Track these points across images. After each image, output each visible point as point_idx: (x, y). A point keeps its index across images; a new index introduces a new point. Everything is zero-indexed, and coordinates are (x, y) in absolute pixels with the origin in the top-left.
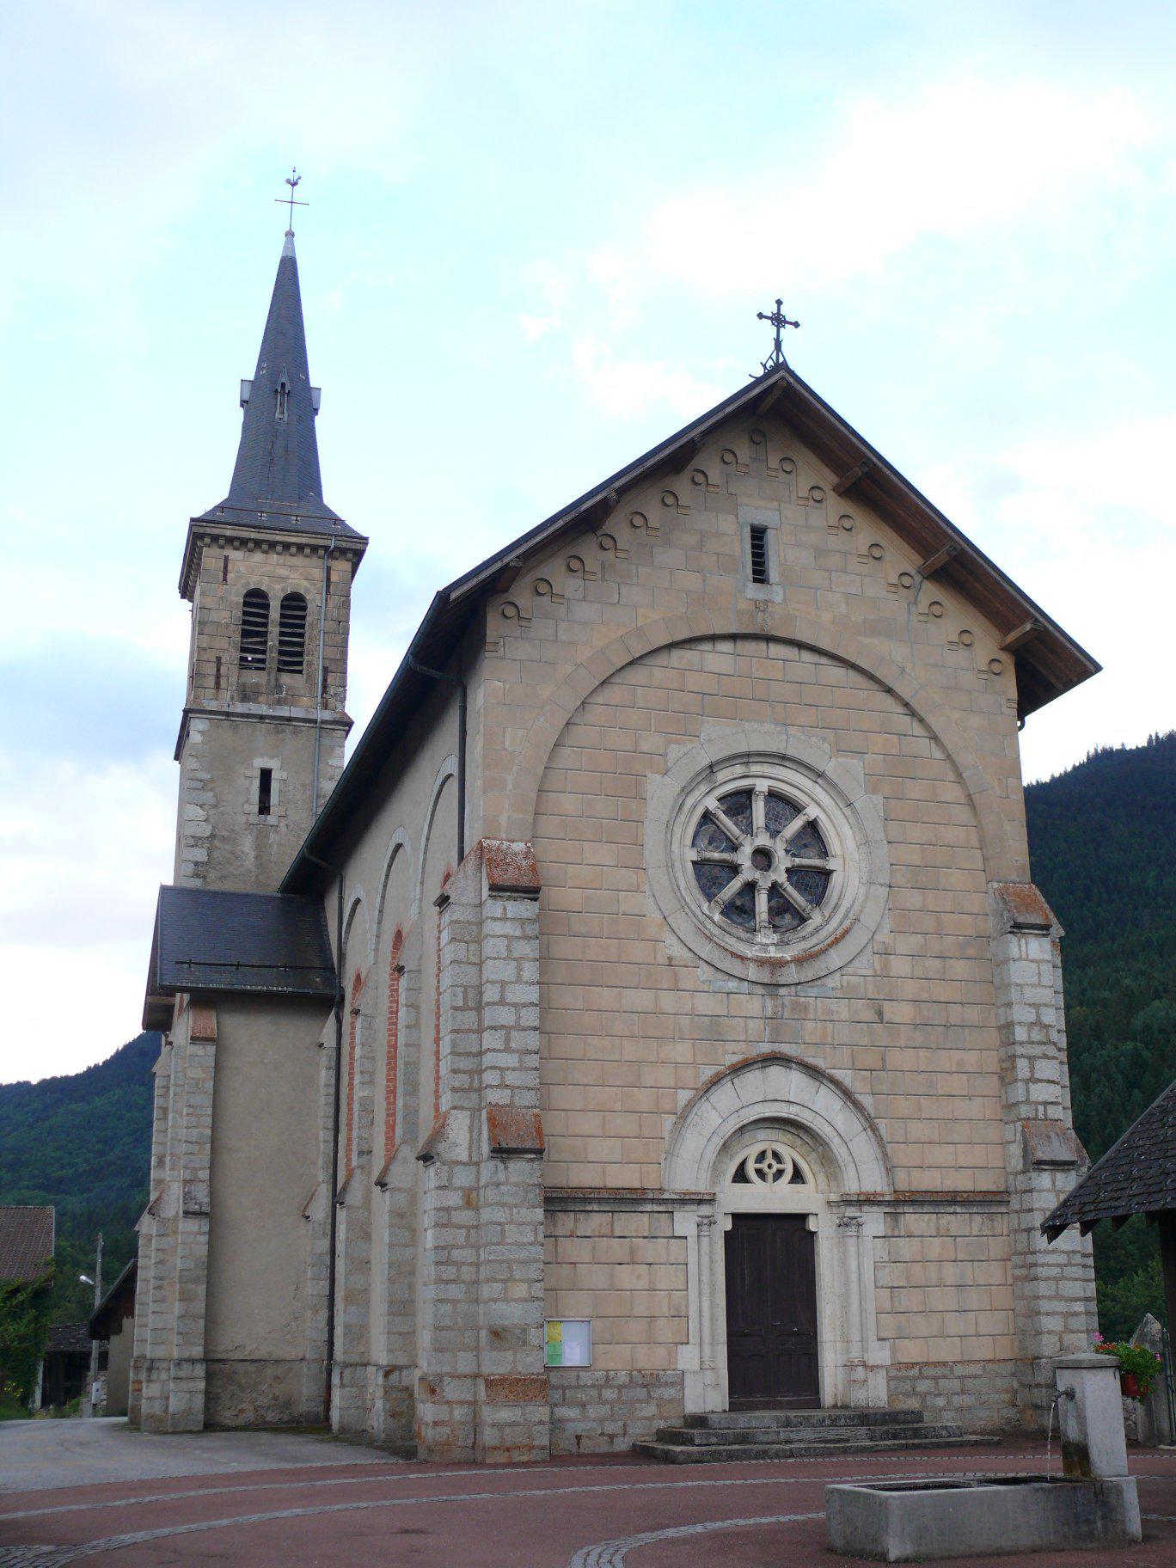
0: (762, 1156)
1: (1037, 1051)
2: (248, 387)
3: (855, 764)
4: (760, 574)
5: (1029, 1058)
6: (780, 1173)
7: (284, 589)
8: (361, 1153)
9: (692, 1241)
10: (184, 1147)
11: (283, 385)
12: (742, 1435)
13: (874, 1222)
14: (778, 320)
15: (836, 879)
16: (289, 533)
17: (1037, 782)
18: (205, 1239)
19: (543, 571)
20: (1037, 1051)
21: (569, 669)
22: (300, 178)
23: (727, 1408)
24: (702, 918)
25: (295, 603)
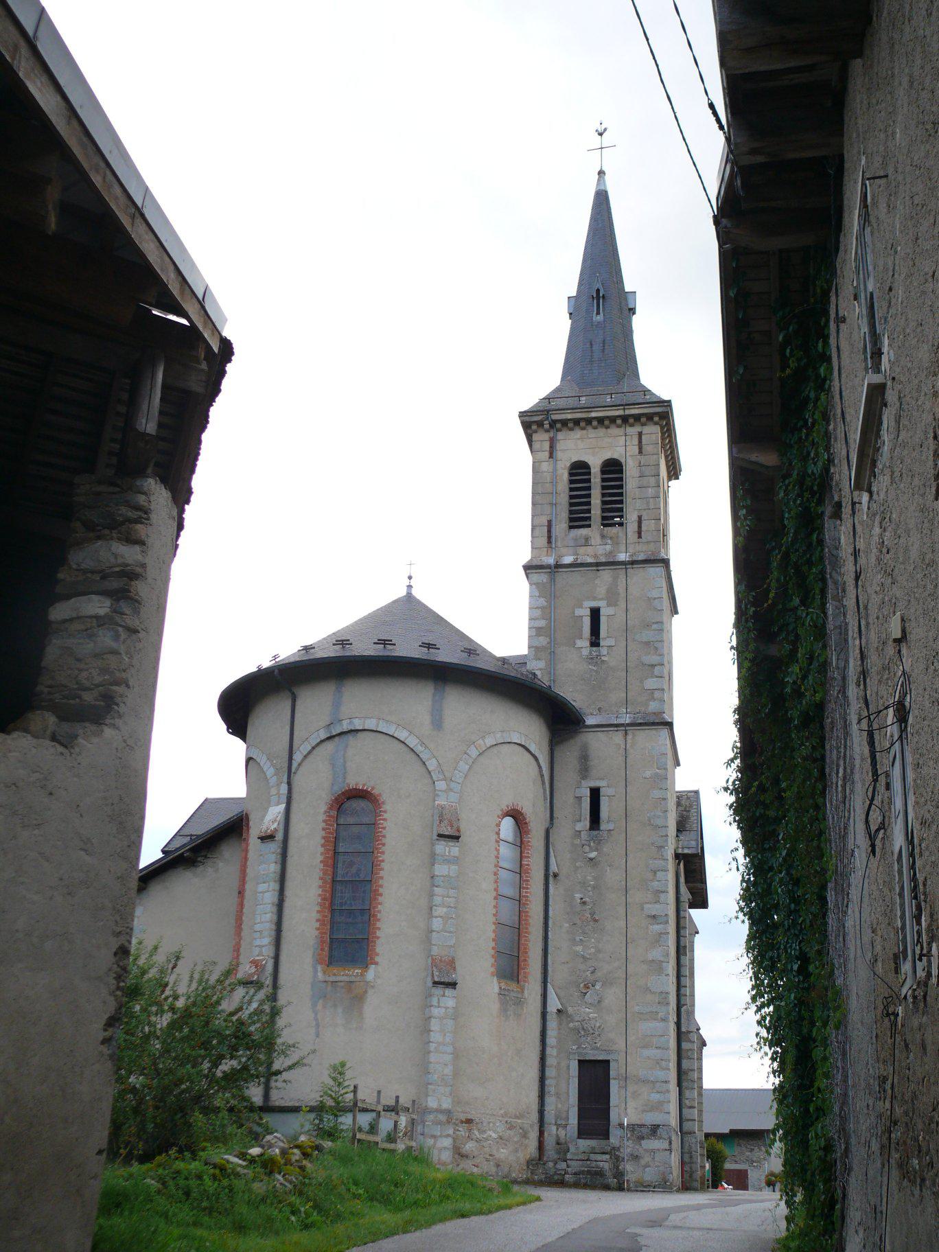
2: (573, 301)
11: (598, 291)
16: (616, 408)
22: (605, 130)
25: (613, 468)
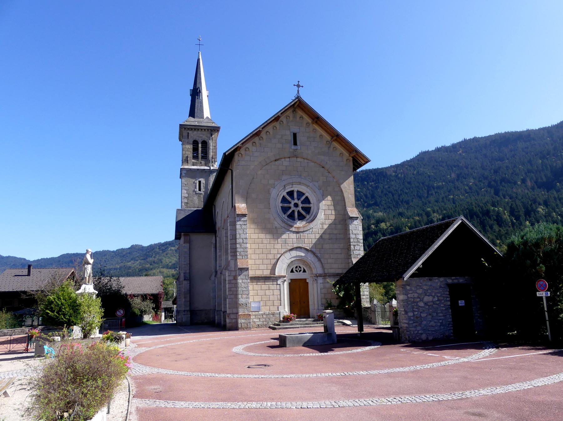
0: (296, 267)
1: (355, 244)
3: (316, 184)
4: (295, 143)
5: (354, 245)
6: (300, 271)
7: (202, 140)
8: (219, 266)
9: (282, 285)
10: (183, 266)
12: (394, 315)
13: (320, 280)
14: (298, 86)
15: (312, 209)
17: (464, 139)
18: (189, 285)
19: (247, 146)
20: (355, 244)
21: (253, 167)
23: (82, 337)
24: (283, 218)
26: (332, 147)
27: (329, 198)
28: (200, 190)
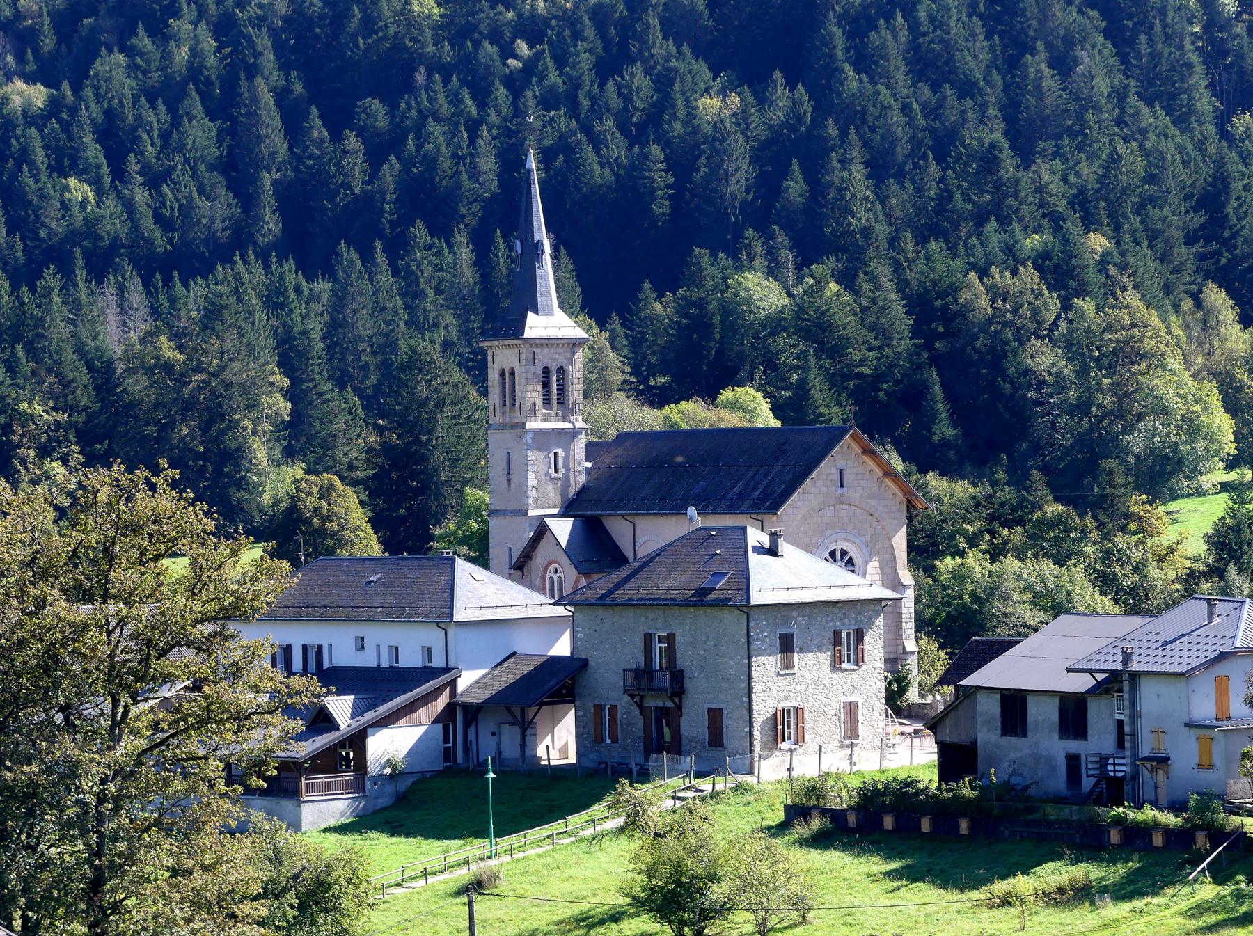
3: (864, 539)
4: (841, 485)
26: (883, 486)
27: (876, 558)
28: (556, 471)
